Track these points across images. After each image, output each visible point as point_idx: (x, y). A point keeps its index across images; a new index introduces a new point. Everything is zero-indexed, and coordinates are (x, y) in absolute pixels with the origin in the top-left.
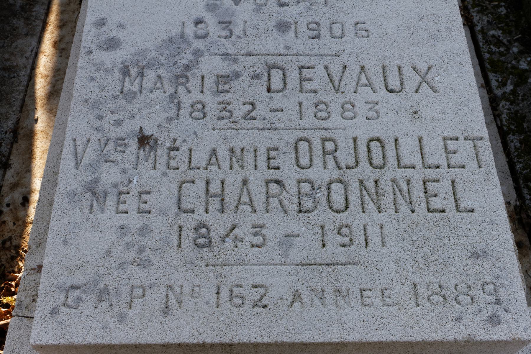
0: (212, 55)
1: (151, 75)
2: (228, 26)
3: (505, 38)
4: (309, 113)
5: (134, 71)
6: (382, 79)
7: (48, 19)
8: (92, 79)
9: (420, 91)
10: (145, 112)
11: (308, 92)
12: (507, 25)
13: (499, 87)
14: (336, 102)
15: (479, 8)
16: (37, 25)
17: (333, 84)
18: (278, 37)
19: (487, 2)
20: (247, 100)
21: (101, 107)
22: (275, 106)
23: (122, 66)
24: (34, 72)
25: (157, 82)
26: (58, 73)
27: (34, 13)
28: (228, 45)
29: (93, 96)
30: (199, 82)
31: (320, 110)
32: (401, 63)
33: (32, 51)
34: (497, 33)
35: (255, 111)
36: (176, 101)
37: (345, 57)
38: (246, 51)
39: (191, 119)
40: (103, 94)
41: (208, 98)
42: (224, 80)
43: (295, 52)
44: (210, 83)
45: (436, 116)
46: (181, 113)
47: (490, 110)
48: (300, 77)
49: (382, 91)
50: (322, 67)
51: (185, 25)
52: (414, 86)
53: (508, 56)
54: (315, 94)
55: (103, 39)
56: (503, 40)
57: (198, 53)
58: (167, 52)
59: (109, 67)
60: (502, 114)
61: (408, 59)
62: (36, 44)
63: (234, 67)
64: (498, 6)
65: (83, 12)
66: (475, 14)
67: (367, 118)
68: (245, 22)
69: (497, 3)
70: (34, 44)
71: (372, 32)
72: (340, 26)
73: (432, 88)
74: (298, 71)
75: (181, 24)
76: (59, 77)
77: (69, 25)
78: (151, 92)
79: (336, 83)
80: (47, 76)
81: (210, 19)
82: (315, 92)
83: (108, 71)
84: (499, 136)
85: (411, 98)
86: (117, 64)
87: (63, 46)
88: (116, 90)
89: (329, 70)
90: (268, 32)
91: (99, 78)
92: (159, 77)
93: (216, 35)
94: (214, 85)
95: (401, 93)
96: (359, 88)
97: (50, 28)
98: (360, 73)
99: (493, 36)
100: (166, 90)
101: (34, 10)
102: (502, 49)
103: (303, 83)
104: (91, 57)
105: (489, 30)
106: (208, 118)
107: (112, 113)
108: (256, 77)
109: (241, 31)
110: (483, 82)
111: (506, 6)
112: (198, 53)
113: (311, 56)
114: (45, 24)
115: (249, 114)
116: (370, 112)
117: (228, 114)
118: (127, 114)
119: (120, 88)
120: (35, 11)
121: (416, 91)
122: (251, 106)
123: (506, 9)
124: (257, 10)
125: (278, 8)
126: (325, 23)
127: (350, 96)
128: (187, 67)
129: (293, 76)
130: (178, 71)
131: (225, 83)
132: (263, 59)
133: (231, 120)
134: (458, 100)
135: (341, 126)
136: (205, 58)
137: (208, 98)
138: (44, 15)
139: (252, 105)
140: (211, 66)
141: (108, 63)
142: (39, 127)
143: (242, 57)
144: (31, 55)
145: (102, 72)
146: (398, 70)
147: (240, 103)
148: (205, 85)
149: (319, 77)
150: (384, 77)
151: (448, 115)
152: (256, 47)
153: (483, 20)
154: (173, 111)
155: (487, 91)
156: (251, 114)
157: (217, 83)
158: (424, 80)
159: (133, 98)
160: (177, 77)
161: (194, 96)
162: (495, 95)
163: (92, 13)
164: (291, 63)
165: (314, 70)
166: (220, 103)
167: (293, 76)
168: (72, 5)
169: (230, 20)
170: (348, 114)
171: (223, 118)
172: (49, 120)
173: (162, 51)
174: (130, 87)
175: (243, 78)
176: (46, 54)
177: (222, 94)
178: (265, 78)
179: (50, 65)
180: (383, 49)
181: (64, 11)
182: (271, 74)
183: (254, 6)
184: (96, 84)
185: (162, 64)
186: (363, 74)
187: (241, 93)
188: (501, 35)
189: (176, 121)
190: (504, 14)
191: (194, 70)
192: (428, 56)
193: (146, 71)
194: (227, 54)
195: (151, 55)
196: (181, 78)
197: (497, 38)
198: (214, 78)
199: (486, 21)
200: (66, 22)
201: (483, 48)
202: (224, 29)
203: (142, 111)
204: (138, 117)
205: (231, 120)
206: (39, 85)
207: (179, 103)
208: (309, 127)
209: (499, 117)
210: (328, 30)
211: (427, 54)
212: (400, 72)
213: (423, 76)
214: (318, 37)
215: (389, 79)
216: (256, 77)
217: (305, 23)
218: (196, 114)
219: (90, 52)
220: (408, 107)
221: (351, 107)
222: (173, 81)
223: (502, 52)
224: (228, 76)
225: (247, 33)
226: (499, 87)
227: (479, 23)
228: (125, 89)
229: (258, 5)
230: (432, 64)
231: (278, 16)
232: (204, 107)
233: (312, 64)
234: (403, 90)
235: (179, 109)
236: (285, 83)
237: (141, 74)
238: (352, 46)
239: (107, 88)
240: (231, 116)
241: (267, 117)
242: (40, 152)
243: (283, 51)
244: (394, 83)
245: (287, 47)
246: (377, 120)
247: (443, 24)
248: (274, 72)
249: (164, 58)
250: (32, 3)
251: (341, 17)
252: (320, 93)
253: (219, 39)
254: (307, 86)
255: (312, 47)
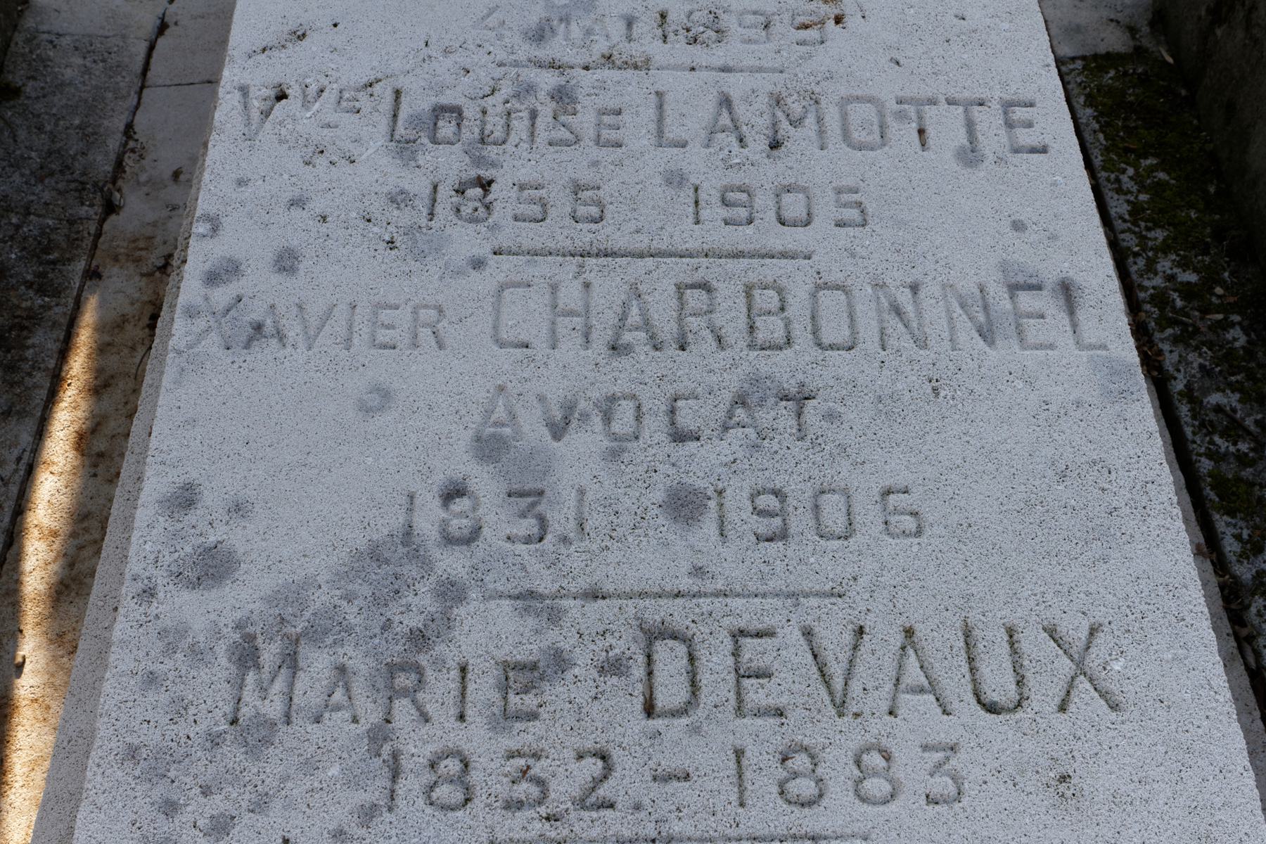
0: (491, 597)
1: (318, 663)
2: (533, 505)
3: (1249, 415)
4: (763, 785)
5: (270, 653)
6: (965, 669)
7: (66, 368)
8: (152, 679)
9: (1072, 708)
10: (296, 790)
11: (759, 713)
12: (1251, 376)
13: (1243, 556)
14: (838, 742)
15: (1177, 330)
16: (35, 386)
17: (827, 684)
18: (672, 537)
19: (1197, 313)
20: (589, 745)
21: (172, 774)
22: (670, 762)
23: (237, 636)
24: (22, 522)
25: (336, 685)
26: (86, 524)
27: (31, 351)
28: (534, 566)
29: (152, 737)
30: (454, 686)
31: (795, 775)
32: (1015, 619)
33: (19, 459)
34: (1228, 399)
35: (612, 781)
36: (386, 750)
37: (858, 598)
38: (583, 583)
39: (429, 810)
40: (182, 729)
41: (478, 739)
42: (523, 675)
43: (719, 587)
44: (483, 689)
45: (1123, 788)
46: (402, 787)
47: (1226, 620)
48: (737, 662)
49: (968, 709)
50: (797, 634)
51: (417, 502)
52: (1057, 692)
53: (1260, 466)
54: (778, 720)
55: (188, 549)
56: (1243, 419)
57: (451, 593)
58: (366, 590)
59: (202, 639)
60: (1259, 634)
61: (1032, 603)
62: (31, 439)
63: (552, 636)
64: (1225, 325)
65: (150, 391)
66: (1166, 347)
67: (931, 800)
68: (582, 492)
69: (1220, 317)
70: (26, 438)
71: (931, 519)
72: (843, 499)
73: (1104, 695)
74: (728, 644)
75: (404, 500)
76: (87, 537)
77: (121, 385)
78: (318, 720)
79: (838, 683)
80: (54, 534)
81: (486, 484)
82: (780, 713)
83: (197, 654)
84: (1253, 699)
85: (1050, 732)
86: (225, 630)
87: (101, 445)
88: (218, 714)
89: (816, 640)
90: (644, 524)
91: (171, 675)
92: (342, 669)
93: (503, 535)
94: (496, 696)
95: (1020, 714)
96: (904, 697)
97: (69, 393)
98: (903, 648)
99: (1218, 409)
100: (360, 712)
101: (30, 342)
102: (1243, 447)
103: (746, 683)
104: (153, 610)
105: (1206, 392)
106: (478, 803)
107: (205, 794)
108: (613, 667)
109: (571, 519)
110: (1202, 540)
111: (1246, 323)
112: (451, 593)
113: (764, 596)
114: (56, 381)
115: (593, 789)
116: (937, 779)
117: (535, 791)
118: (247, 796)
119: (228, 709)
120: (33, 346)
121: (1062, 708)
122: (600, 763)
123: (1247, 335)
124: (614, 455)
125: (670, 448)
126: (799, 492)
127: (878, 726)
128: (419, 639)
129: (716, 663)
130: (396, 651)
131: (526, 691)
132: (630, 607)
133: (543, 811)
134: (1182, 737)
135: (856, 827)
136: (471, 608)
137: (478, 739)
138: (56, 356)
139: (603, 758)
140: (489, 632)
141: (199, 627)
142: (27, 685)
143: (572, 602)
144: (16, 471)
145: (179, 656)
146: (1006, 638)
147: (569, 754)
148: (469, 698)
149: (791, 678)
150: (971, 660)
151: (1155, 786)
152: (612, 572)
153: (1188, 363)
154: (378, 783)
155: (1212, 562)
156: (601, 792)
157: (504, 688)
158: (1081, 669)
159: (266, 742)
160: (393, 669)
161: (439, 733)
162: (1234, 577)
163: (161, 467)
164: (710, 621)
165: (775, 642)
166: (511, 755)
167: (716, 663)
168: (129, 327)
169: (539, 486)
170: (877, 786)
171: (520, 805)
172: (53, 668)
173: (350, 587)
174: (258, 703)
175: (576, 671)
176: (55, 469)
177: (519, 725)
178: (638, 672)
179: (64, 500)
180: (964, 572)
181: (109, 344)
182: (655, 657)
183: (606, 443)
184: (164, 698)
185: (349, 630)
186: (911, 652)
187: (570, 720)
188: (1239, 406)
189: (387, 816)
190: (1243, 347)
191: (440, 648)
192: (1088, 594)
193: (305, 650)
194: (532, 594)
195: (320, 599)
196: (401, 675)
197: (1228, 416)
198: (497, 672)
199: (1195, 365)
200: (112, 377)
201: (1194, 442)
202: (523, 515)
203: (289, 785)
204: (277, 804)
205: (543, 811)
206: (33, 559)
207: (395, 756)
208: (766, 832)
209: (1250, 644)
210: (809, 515)
211: (1084, 589)
212: (1012, 644)
213: (1076, 656)
214: (782, 535)
215: (985, 670)
216: (613, 667)
217: (746, 494)
218: (445, 792)
219: (149, 593)
220: (1041, 760)
221: (883, 763)
222: (380, 684)
223: (1246, 455)
224: (534, 667)
225: (587, 529)
226: (1243, 556)
227: (1179, 371)
228: (244, 710)
229: (616, 438)
230: (1101, 620)
231: (671, 471)
232: (466, 766)
233: (767, 622)
234: (1025, 704)
235: (395, 775)
236: (694, 685)
237: (291, 661)
238: (876, 566)
239: (192, 710)
240: (544, 794)
241: (646, 801)
242: (23, 765)
243: (685, 583)
244: (1000, 685)
245: (698, 571)
246: (957, 806)
247: (1122, 492)
248: (662, 650)
249: (356, 610)
250: (26, 323)
251: (844, 473)
252: (793, 717)
253: (508, 545)
254: (756, 694)
255: (766, 569)
